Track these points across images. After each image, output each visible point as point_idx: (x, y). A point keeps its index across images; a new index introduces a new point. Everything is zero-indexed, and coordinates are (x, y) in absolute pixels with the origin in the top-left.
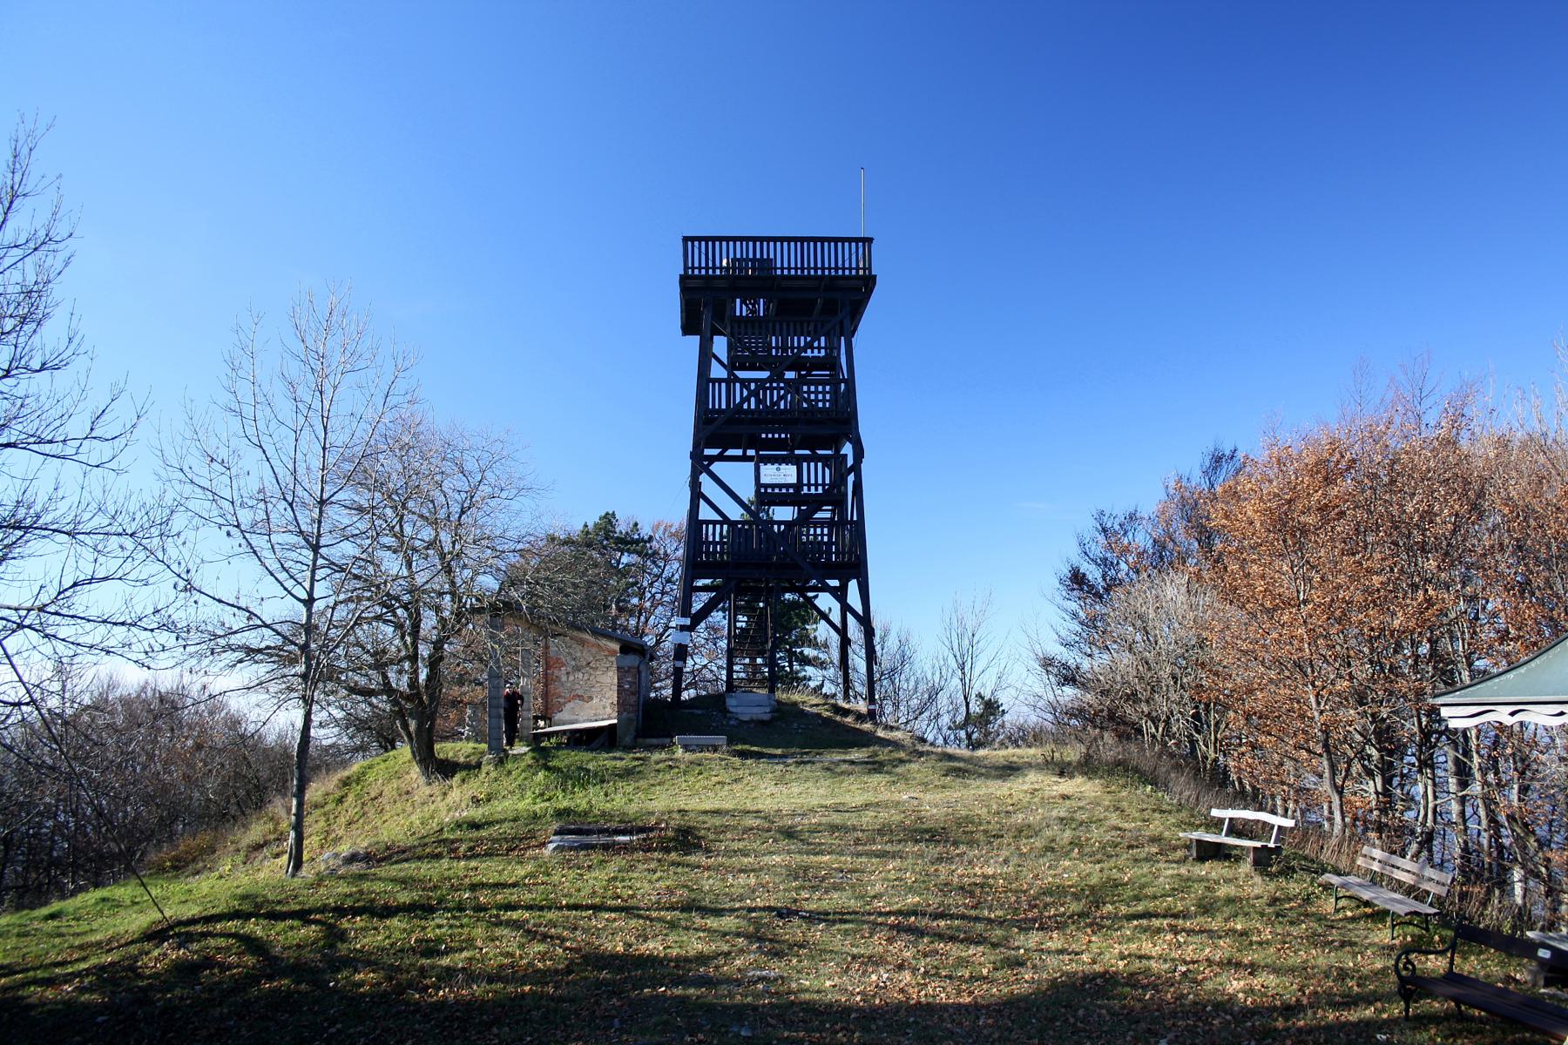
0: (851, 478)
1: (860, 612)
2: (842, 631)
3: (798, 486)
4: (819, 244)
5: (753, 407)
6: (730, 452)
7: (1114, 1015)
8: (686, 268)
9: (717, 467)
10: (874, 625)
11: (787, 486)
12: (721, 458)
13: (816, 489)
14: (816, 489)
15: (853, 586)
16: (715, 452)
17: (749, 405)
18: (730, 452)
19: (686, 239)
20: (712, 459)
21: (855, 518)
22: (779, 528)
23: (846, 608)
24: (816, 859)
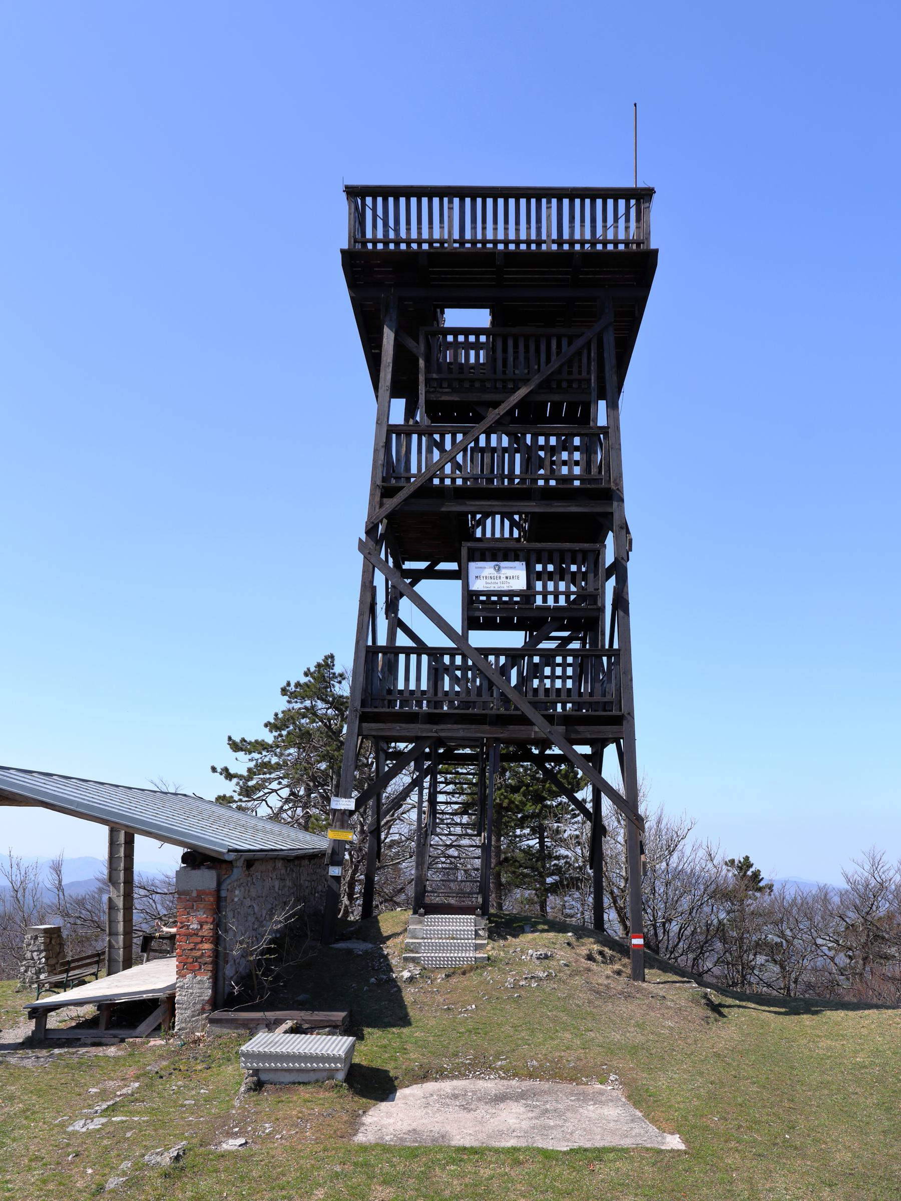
0: (611, 584)
1: (622, 791)
2: (595, 817)
3: (528, 596)
4: (566, 202)
5: (448, 437)
6: (443, 566)
7: (309, 790)
8: (353, 239)
9: (424, 588)
10: (641, 811)
11: (511, 594)
12: (431, 574)
13: (556, 600)
14: (556, 600)
15: (610, 753)
16: (422, 565)
17: (484, 532)
18: (443, 566)
19: (354, 193)
20: (417, 576)
21: (616, 646)
22: (497, 661)
23: (601, 788)
24: (485, 1085)
